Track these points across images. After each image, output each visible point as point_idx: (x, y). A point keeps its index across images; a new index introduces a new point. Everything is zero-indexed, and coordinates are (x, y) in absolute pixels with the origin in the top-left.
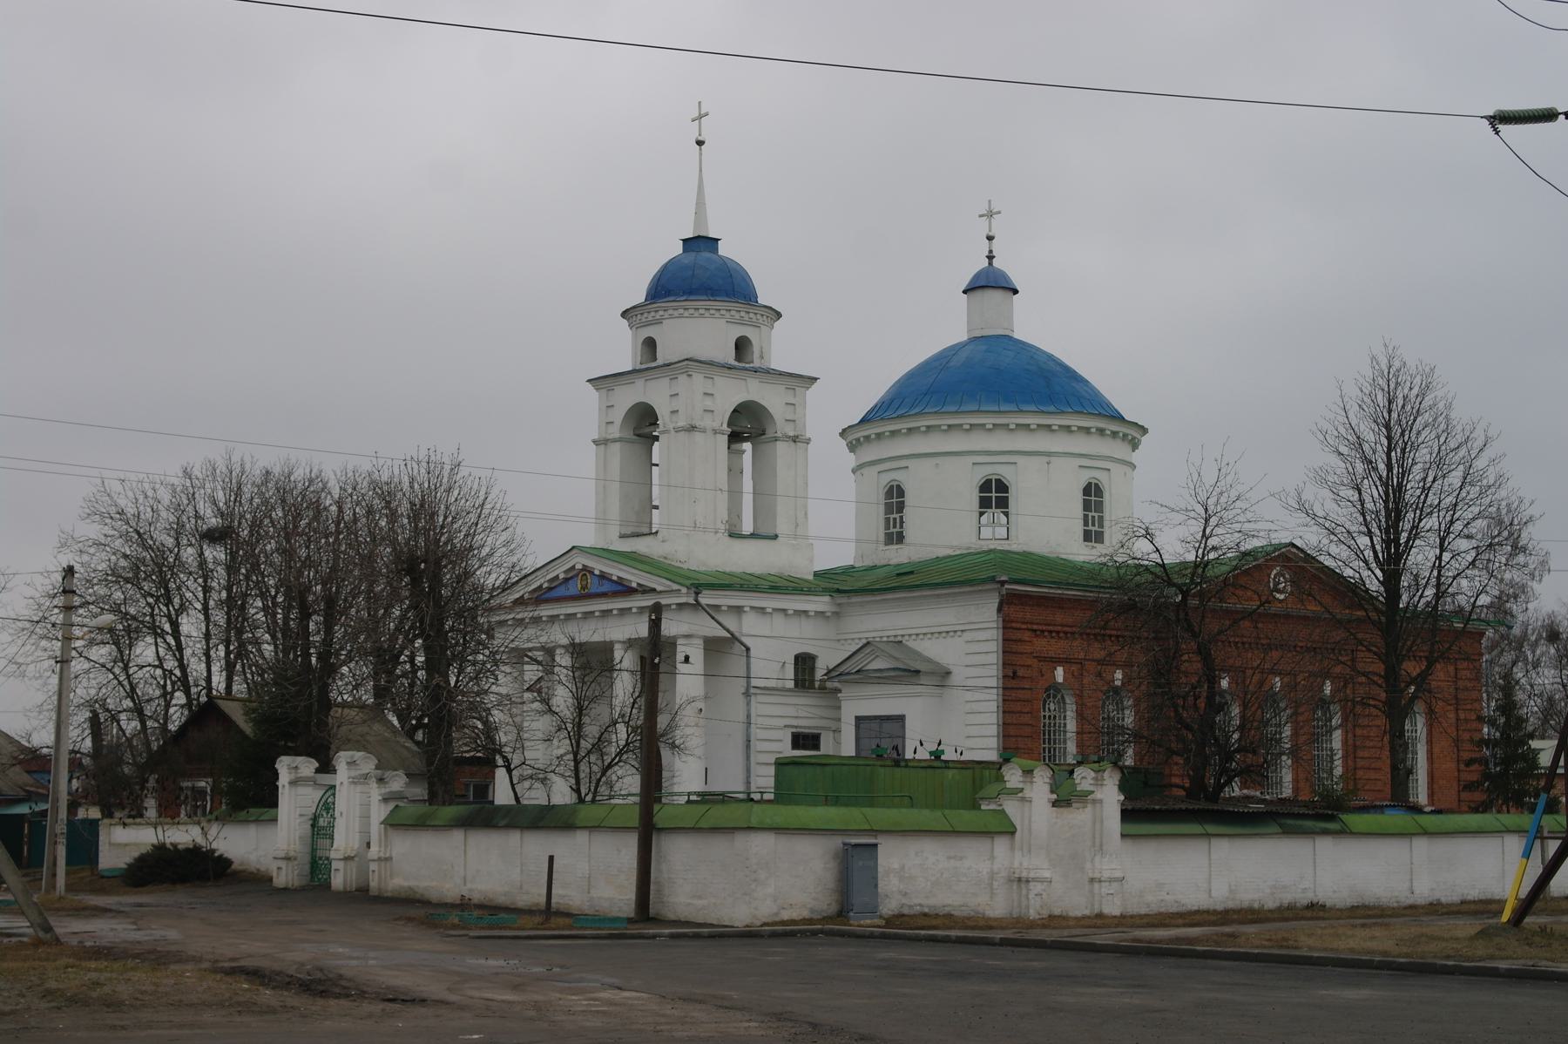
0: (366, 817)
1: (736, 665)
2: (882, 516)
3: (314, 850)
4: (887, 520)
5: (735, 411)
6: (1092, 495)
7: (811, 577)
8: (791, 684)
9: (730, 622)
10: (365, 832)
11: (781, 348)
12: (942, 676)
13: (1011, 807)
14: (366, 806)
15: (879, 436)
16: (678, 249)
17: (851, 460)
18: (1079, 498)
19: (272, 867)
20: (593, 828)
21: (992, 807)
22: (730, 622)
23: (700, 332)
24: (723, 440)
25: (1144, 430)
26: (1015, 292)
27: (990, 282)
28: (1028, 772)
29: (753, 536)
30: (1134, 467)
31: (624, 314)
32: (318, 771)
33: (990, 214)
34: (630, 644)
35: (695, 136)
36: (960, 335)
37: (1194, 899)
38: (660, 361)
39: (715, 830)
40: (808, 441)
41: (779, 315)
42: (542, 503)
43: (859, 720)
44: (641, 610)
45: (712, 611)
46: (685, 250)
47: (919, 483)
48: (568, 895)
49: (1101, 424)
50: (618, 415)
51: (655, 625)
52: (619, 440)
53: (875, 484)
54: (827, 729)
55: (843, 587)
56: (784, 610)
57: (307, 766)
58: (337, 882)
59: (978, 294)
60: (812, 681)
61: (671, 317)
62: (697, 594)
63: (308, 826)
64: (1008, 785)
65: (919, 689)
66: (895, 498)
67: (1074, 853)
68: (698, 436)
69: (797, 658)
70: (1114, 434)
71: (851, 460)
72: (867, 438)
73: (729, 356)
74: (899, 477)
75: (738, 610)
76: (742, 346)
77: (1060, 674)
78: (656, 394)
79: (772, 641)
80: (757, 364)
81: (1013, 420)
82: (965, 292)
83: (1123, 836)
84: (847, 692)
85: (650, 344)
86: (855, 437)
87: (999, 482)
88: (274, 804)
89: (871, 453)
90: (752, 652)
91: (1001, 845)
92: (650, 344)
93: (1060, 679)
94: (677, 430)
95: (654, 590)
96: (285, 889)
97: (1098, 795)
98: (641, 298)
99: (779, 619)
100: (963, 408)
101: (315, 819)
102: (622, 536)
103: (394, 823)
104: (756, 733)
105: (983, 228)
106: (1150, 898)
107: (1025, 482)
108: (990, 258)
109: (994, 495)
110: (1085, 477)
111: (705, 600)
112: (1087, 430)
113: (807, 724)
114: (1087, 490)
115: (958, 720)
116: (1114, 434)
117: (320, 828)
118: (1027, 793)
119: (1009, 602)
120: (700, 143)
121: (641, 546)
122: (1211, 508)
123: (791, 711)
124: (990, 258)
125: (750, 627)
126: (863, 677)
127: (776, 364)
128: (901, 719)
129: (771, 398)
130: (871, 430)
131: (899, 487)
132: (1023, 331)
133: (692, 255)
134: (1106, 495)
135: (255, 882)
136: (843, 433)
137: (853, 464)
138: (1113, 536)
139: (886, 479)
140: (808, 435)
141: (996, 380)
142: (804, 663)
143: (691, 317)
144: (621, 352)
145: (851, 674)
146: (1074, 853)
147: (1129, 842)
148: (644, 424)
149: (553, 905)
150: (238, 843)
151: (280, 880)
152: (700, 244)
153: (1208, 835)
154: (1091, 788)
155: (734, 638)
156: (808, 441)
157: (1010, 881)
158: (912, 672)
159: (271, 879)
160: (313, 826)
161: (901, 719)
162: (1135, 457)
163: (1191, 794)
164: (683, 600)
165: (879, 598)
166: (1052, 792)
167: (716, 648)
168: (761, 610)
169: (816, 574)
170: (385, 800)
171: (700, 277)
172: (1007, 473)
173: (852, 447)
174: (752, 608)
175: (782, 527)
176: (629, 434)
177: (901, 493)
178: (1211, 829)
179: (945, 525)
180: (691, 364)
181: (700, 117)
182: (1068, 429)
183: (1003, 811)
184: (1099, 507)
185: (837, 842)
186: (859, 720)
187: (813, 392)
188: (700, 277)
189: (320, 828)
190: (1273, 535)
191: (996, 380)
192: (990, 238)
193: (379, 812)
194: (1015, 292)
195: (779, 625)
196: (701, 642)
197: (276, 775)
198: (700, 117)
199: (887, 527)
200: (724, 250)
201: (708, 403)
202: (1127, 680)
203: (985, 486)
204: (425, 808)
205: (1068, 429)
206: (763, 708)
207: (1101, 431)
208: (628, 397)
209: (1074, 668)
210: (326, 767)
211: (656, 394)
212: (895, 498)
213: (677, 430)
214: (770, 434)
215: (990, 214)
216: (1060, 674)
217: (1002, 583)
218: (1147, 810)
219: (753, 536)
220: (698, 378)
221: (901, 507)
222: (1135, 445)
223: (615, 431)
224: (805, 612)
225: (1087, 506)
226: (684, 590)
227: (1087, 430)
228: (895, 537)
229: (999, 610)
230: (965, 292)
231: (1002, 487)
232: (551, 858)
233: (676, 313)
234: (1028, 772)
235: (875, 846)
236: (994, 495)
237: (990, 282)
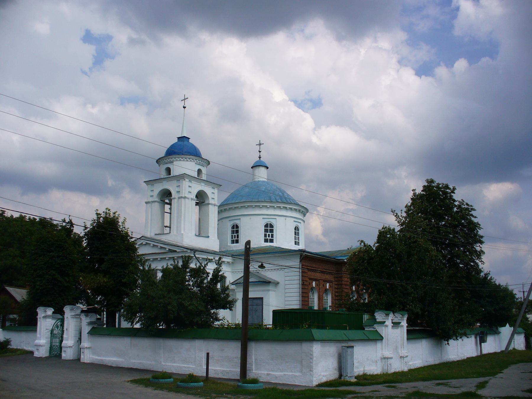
3: (51, 343)
16: (176, 140)
21: (371, 329)
32: (53, 313)
33: (260, 144)
61: (177, 160)
63: (49, 333)
64: (377, 320)
68: (187, 200)
88: (35, 324)
93: (314, 286)
101: (52, 331)
108: (260, 157)
109: (269, 228)
117: (57, 335)
120: (184, 107)
124: (260, 157)
133: (181, 143)
134: (300, 230)
139: (232, 223)
143: (184, 161)
150: (19, 340)
157: (381, 359)
159: (32, 353)
160: (51, 333)
165: (264, 256)
172: (273, 222)
177: (237, 227)
180: (183, 177)
181: (185, 99)
185: (340, 345)
189: (57, 335)
192: (260, 152)
197: (37, 314)
198: (185, 99)
200: (190, 141)
201: (190, 189)
202: (330, 286)
203: (266, 226)
208: (158, 188)
209: (317, 282)
214: (207, 202)
215: (260, 144)
221: (237, 232)
229: (300, 261)
231: (271, 226)
236: (269, 228)
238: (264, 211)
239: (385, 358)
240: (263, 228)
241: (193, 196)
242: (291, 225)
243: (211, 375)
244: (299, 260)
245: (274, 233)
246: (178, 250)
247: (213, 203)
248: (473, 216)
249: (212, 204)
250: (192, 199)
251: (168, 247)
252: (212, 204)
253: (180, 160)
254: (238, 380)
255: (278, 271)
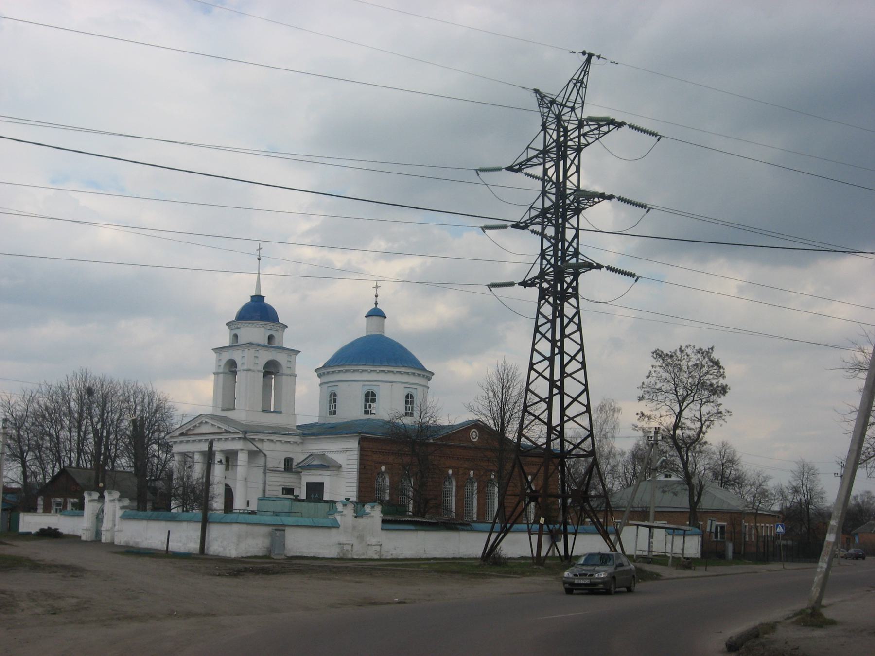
0: (114, 515)
9: (259, 445)
10: (114, 521)
11: (288, 340)
12: (339, 467)
13: (338, 518)
14: (114, 512)
17: (319, 381)
18: (404, 399)
19: (79, 533)
22: (259, 445)
23: (255, 332)
25: (433, 374)
27: (376, 313)
28: (373, 507)
29: (274, 412)
31: (227, 324)
33: (377, 287)
34: (202, 453)
36: (363, 334)
37: (438, 554)
41: (286, 327)
42: (191, 396)
44: (206, 440)
45: (252, 441)
48: (176, 546)
49: (418, 372)
50: (223, 363)
53: (327, 391)
55: (310, 432)
57: (96, 495)
58: (103, 539)
65: (328, 472)
67: (370, 536)
70: (419, 375)
71: (319, 381)
75: (262, 440)
76: (270, 338)
78: (237, 355)
79: (276, 452)
81: (378, 369)
86: (321, 372)
95: (230, 432)
96: (86, 542)
99: (278, 444)
102: (223, 410)
103: (124, 517)
104: (268, 487)
106: (394, 552)
108: (376, 304)
109: (370, 397)
110: (407, 391)
113: (289, 485)
114: (407, 397)
115: (342, 486)
116: (419, 375)
117: (99, 518)
119: (363, 441)
120: (259, 259)
121: (229, 414)
124: (376, 304)
125: (266, 447)
126: (309, 467)
128: (322, 484)
129: (281, 358)
132: (388, 333)
135: (74, 539)
136: (316, 371)
141: (376, 351)
142: (288, 462)
144: (225, 340)
145: (307, 467)
146: (370, 536)
151: (84, 538)
152: (258, 299)
153: (416, 530)
155: (260, 451)
158: (327, 465)
159: (80, 537)
161: (322, 484)
162: (430, 384)
169: (298, 426)
170: (122, 508)
171: (258, 310)
172: (375, 389)
173: (320, 376)
175: (283, 410)
176: (227, 370)
177: (335, 395)
178: (418, 528)
179: (351, 409)
182: (400, 372)
188: (258, 310)
189: (99, 518)
191: (376, 351)
193: (119, 513)
195: (279, 446)
200: (266, 301)
203: (367, 394)
204: (135, 512)
205: (400, 372)
206: (272, 478)
208: (226, 356)
210: (102, 497)
211: (237, 355)
214: (280, 372)
215: (377, 287)
218: (394, 519)
219: (274, 412)
220: (252, 350)
221: (335, 401)
222: (429, 379)
227: (408, 373)
231: (373, 394)
234: (373, 507)
236: (370, 397)
237: (376, 313)
238: (366, 376)
240: (364, 397)
241: (261, 367)
243: (170, 549)
245: (363, 409)
248: (491, 407)
249: (287, 375)
250: (259, 371)
252: (287, 375)
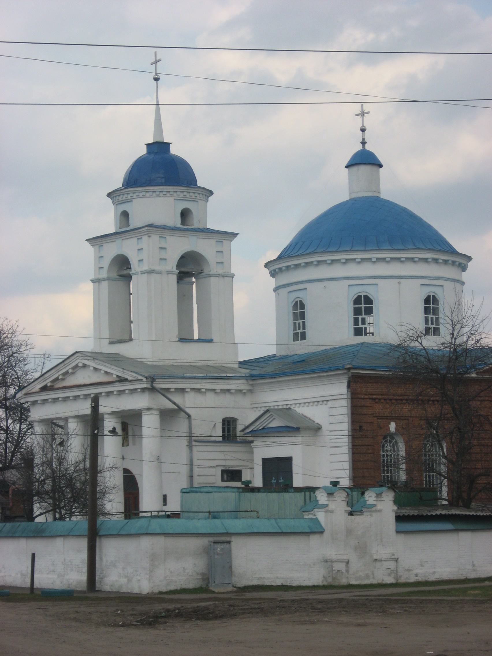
1: (182, 426)
2: (291, 322)
4: (295, 324)
5: (182, 257)
6: (430, 304)
7: (236, 366)
8: (221, 439)
9: (178, 399)
15: (288, 268)
17: (272, 283)
18: (421, 306)
20: (65, 536)
21: (311, 516)
22: (178, 399)
23: (157, 206)
24: (175, 277)
25: (469, 258)
26: (381, 166)
27: (365, 159)
29: (199, 340)
30: (463, 283)
31: (109, 195)
34: (80, 418)
35: (153, 75)
38: (131, 227)
39: (129, 535)
40: (232, 276)
41: (211, 193)
43: (265, 461)
44: (86, 396)
45: (165, 392)
46: (149, 152)
47: (314, 298)
48: (45, 580)
50: (106, 262)
51: (95, 408)
52: (108, 279)
54: (246, 467)
55: (261, 371)
56: (214, 390)
59: (355, 169)
60: (235, 436)
61: (138, 197)
62: (152, 382)
65: (299, 439)
66: (299, 310)
69: (224, 421)
71: (272, 283)
72: (280, 269)
73: (178, 223)
74: (300, 295)
75: (182, 391)
76: (185, 214)
77: (393, 427)
78: (129, 248)
79: (206, 409)
80: (196, 225)
82: (347, 167)
83: (398, 532)
84: (258, 443)
85: (125, 215)
86: (275, 268)
87: (366, 297)
89: (285, 278)
90: (192, 417)
91: (314, 539)
92: (125, 215)
94: (143, 273)
95: (126, 380)
97: (379, 507)
98: (119, 184)
100: (341, 249)
105: (358, 123)
107: (384, 296)
108: (364, 143)
109: (363, 306)
111: (160, 384)
112: (425, 260)
113: (232, 464)
114: (427, 300)
115: (324, 460)
116: (446, 262)
118: (379, 507)
119: (354, 382)
120: (156, 79)
122: (455, 319)
123: (221, 456)
124: (364, 143)
125: (189, 402)
126: (266, 432)
127: (211, 225)
129: (205, 247)
130: (283, 265)
131: (301, 301)
134: (441, 302)
136: (267, 265)
137: (274, 286)
138: (445, 329)
139: (294, 296)
140: (233, 271)
141: (369, 226)
142: (229, 425)
144: (108, 223)
146: (377, 545)
147: (402, 537)
148: (122, 268)
149: (35, 587)
152: (159, 149)
153: (457, 530)
154: (375, 503)
155: (180, 409)
156: (232, 276)
158: (296, 427)
162: (465, 276)
163: (452, 504)
164: (145, 386)
166: (348, 505)
167: (167, 416)
168: (199, 390)
171: (160, 168)
172: (371, 292)
173: (273, 274)
174: (192, 389)
176: (114, 275)
177: (302, 306)
178: (459, 526)
179: (331, 329)
182: (412, 260)
183: (317, 519)
184: (436, 311)
186: (265, 461)
187: (235, 243)
188: (160, 168)
190: (80, 411)
191: (369, 226)
192: (363, 130)
194: (381, 166)
195: (210, 399)
196: (157, 412)
199: (295, 329)
203: (357, 301)
205: (412, 260)
207: (436, 261)
208: (112, 250)
211: (129, 248)
212: (299, 310)
213: (143, 273)
214: (206, 271)
216: (393, 427)
217: (349, 369)
218: (417, 513)
219: (199, 340)
220: (155, 238)
221: (303, 316)
222: (464, 268)
223: (104, 274)
224: (228, 391)
225: (427, 311)
226: (144, 380)
227: (425, 260)
228: (300, 336)
229: (349, 386)
230: (347, 167)
231: (368, 300)
232: (33, 555)
233: (141, 195)
235: (229, 542)
236: (363, 306)
237: (365, 159)
239: (326, 561)
240: (351, 306)
241: (172, 265)
242: (414, 296)
243: (37, 585)
244: (345, 384)
246: (130, 378)
247: (220, 272)
250: (168, 273)
251: (116, 372)
253: (144, 196)
254: (84, 592)
255: (319, 406)
